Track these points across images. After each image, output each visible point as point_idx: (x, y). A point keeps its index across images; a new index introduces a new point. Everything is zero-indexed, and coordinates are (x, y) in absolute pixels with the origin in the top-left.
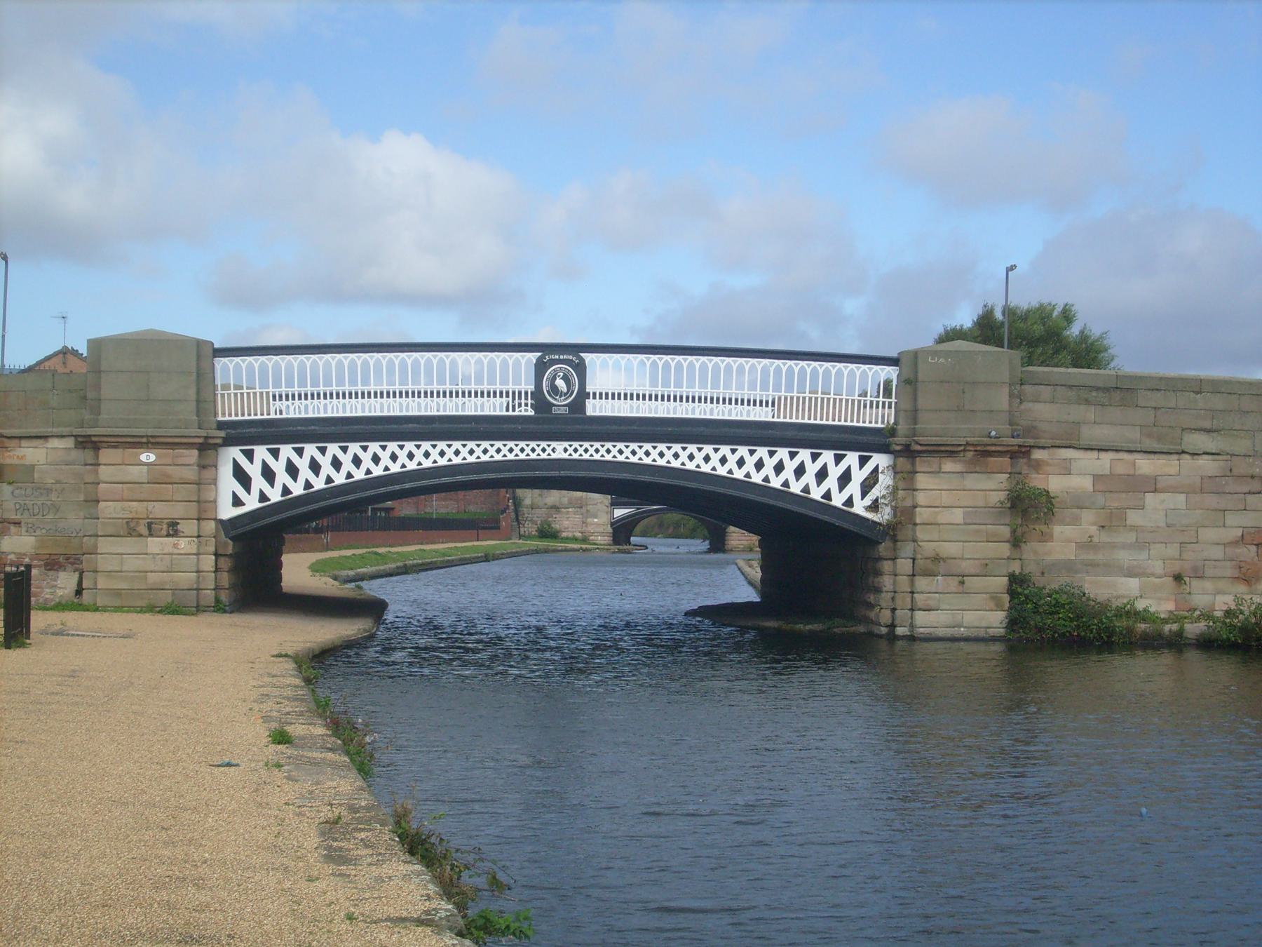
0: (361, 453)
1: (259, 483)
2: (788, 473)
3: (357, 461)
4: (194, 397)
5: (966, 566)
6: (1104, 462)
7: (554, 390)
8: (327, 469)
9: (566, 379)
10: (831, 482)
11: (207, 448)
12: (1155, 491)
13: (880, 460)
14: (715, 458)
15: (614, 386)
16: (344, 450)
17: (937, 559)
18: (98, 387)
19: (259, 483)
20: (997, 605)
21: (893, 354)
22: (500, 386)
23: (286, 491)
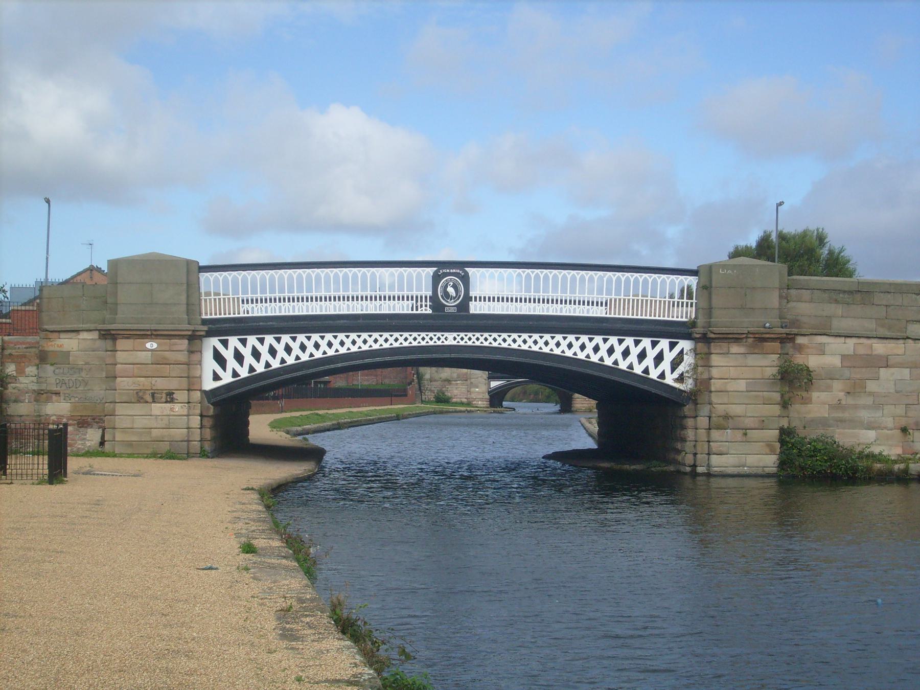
0: (306, 342)
1: (232, 363)
2: (603, 352)
3: (303, 348)
4: (185, 302)
5: (748, 422)
6: (849, 346)
7: (446, 295)
8: (281, 353)
9: (455, 287)
10: (649, 361)
11: (194, 338)
12: (887, 366)
13: (684, 345)
14: (564, 344)
15: (491, 292)
16: (294, 339)
17: (727, 417)
18: (115, 294)
19: (232, 363)
20: (771, 451)
21: (694, 267)
22: (407, 292)
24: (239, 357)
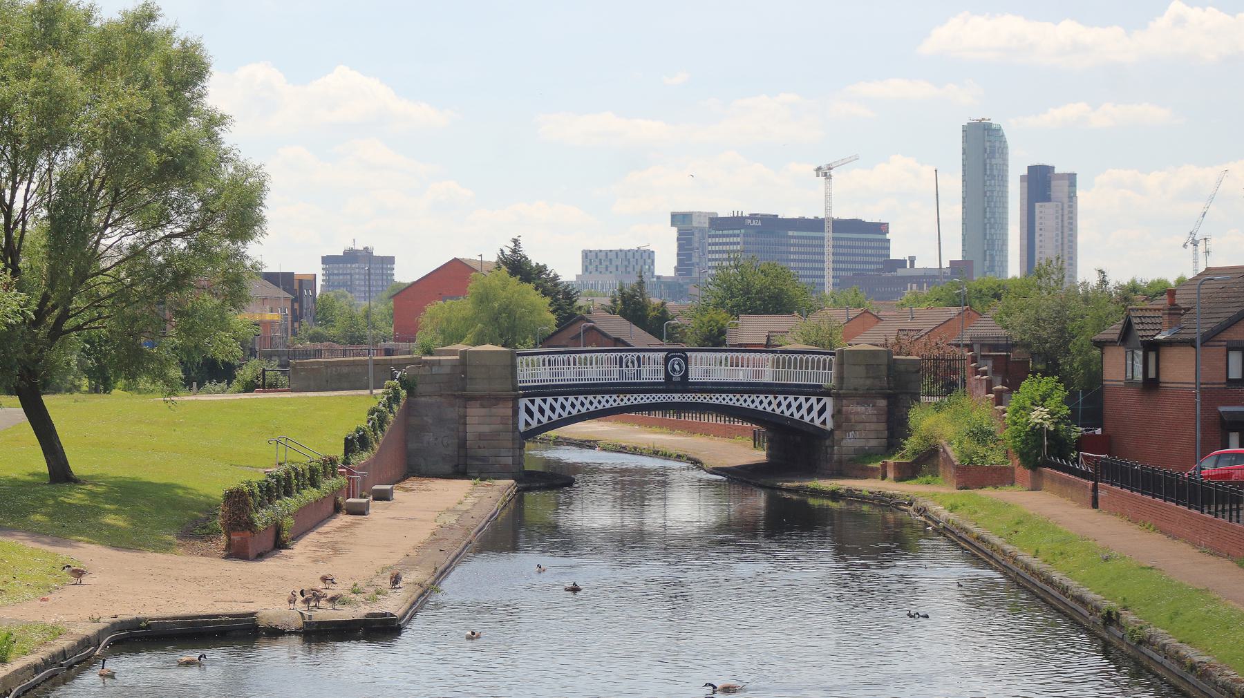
1: (537, 415)
2: (783, 407)
7: (674, 370)
10: (804, 411)
19: (537, 415)
23: (550, 418)
24: (542, 411)
